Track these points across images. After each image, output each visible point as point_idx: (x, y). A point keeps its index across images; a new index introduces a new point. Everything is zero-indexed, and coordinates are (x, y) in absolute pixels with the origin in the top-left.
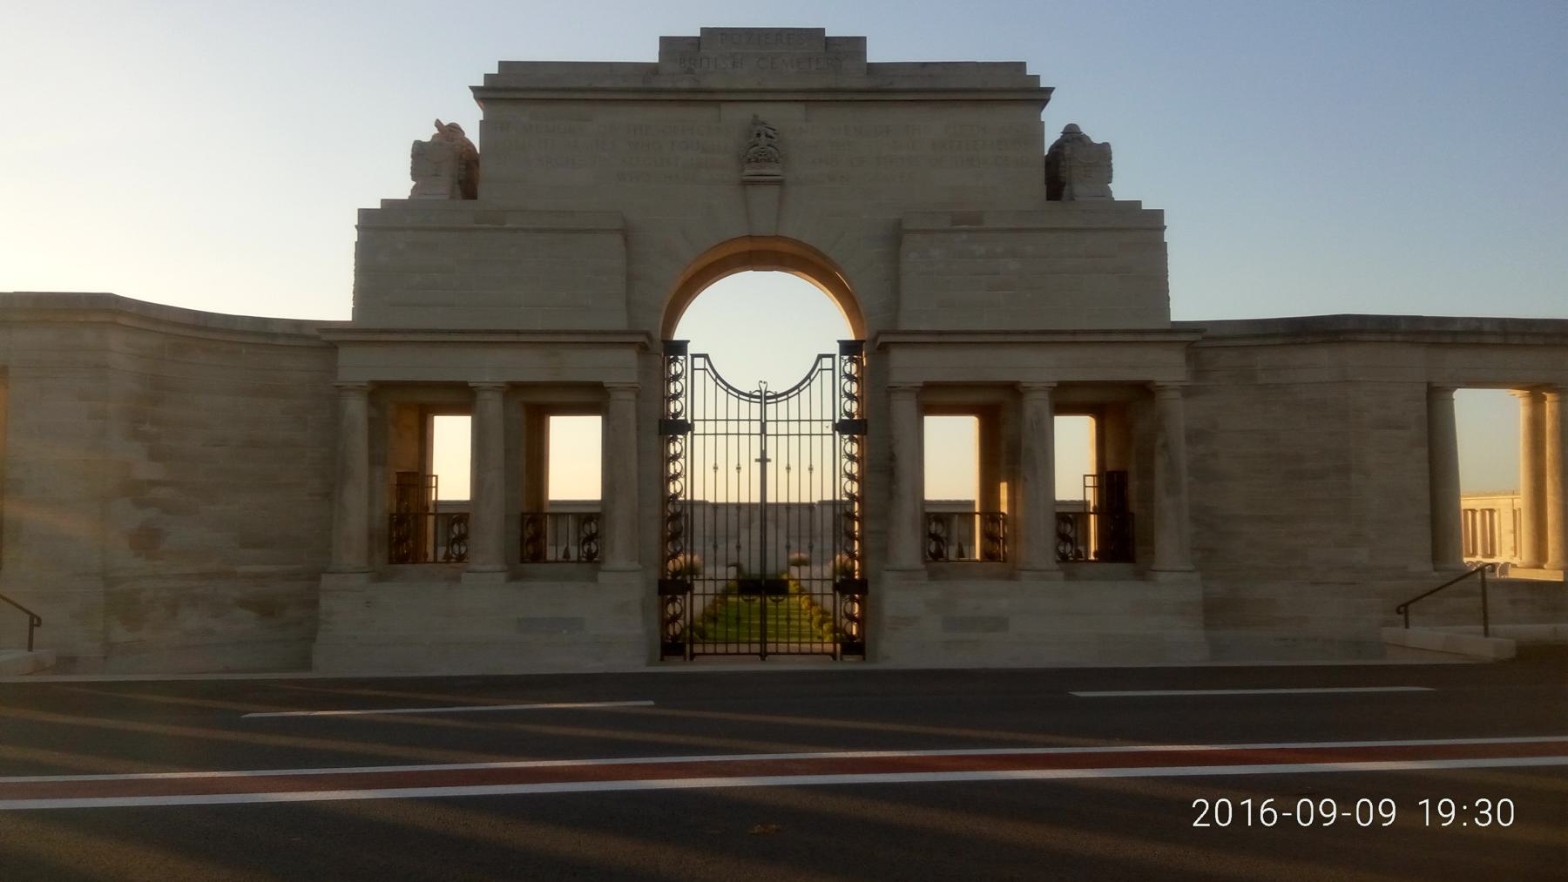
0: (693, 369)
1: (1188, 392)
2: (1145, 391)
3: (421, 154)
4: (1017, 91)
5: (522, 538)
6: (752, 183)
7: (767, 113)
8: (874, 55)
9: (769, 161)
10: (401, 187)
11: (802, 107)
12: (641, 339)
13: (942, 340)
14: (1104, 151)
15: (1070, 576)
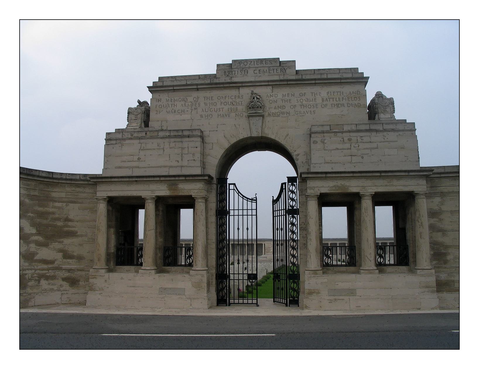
0: (229, 190)
1: (428, 196)
2: (411, 196)
3: (130, 112)
4: (355, 79)
5: (164, 257)
6: (252, 116)
7: (257, 90)
8: (299, 67)
9: (258, 107)
10: (123, 124)
11: (271, 87)
12: (207, 178)
13: (325, 175)
14: (391, 102)
15: (381, 272)
